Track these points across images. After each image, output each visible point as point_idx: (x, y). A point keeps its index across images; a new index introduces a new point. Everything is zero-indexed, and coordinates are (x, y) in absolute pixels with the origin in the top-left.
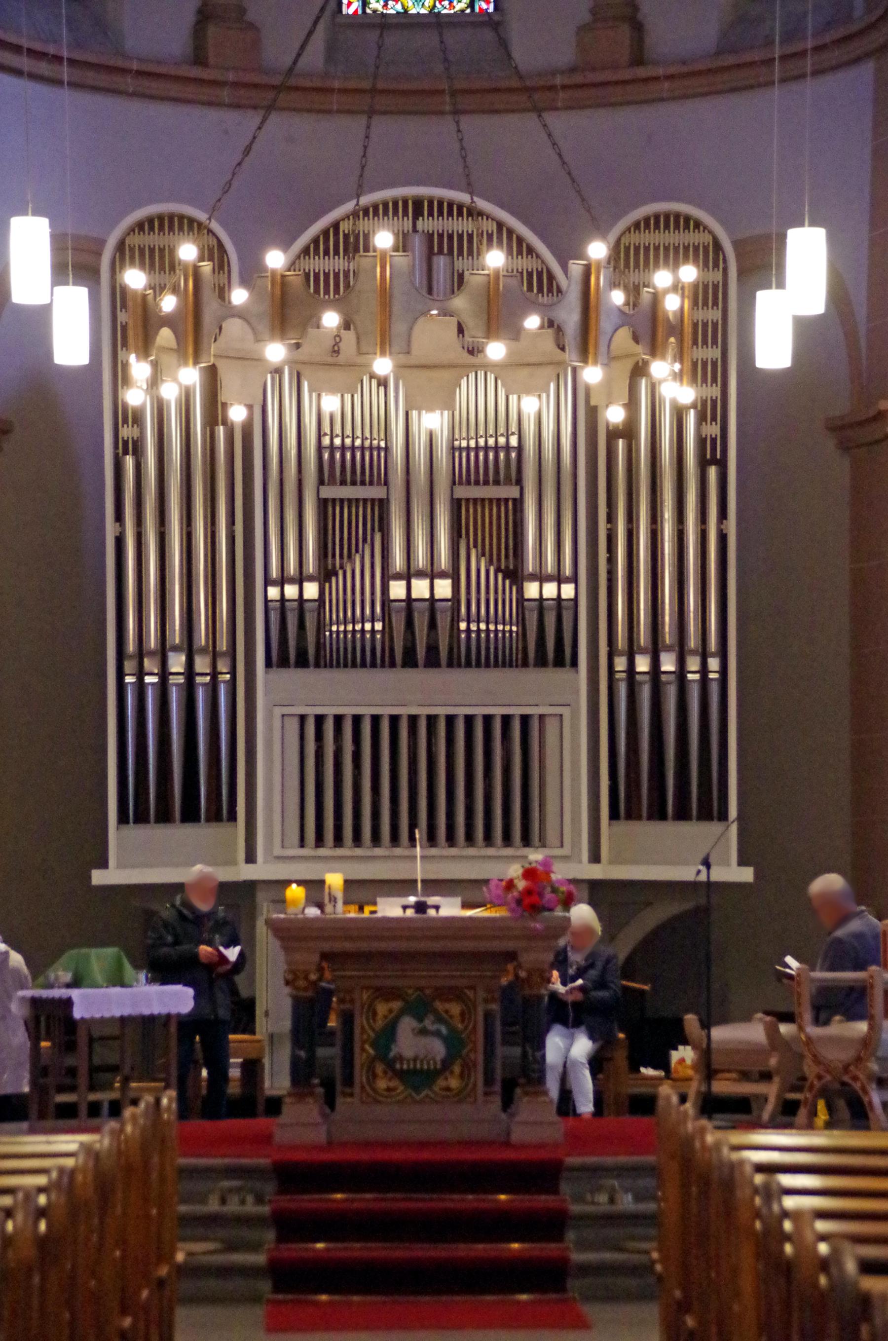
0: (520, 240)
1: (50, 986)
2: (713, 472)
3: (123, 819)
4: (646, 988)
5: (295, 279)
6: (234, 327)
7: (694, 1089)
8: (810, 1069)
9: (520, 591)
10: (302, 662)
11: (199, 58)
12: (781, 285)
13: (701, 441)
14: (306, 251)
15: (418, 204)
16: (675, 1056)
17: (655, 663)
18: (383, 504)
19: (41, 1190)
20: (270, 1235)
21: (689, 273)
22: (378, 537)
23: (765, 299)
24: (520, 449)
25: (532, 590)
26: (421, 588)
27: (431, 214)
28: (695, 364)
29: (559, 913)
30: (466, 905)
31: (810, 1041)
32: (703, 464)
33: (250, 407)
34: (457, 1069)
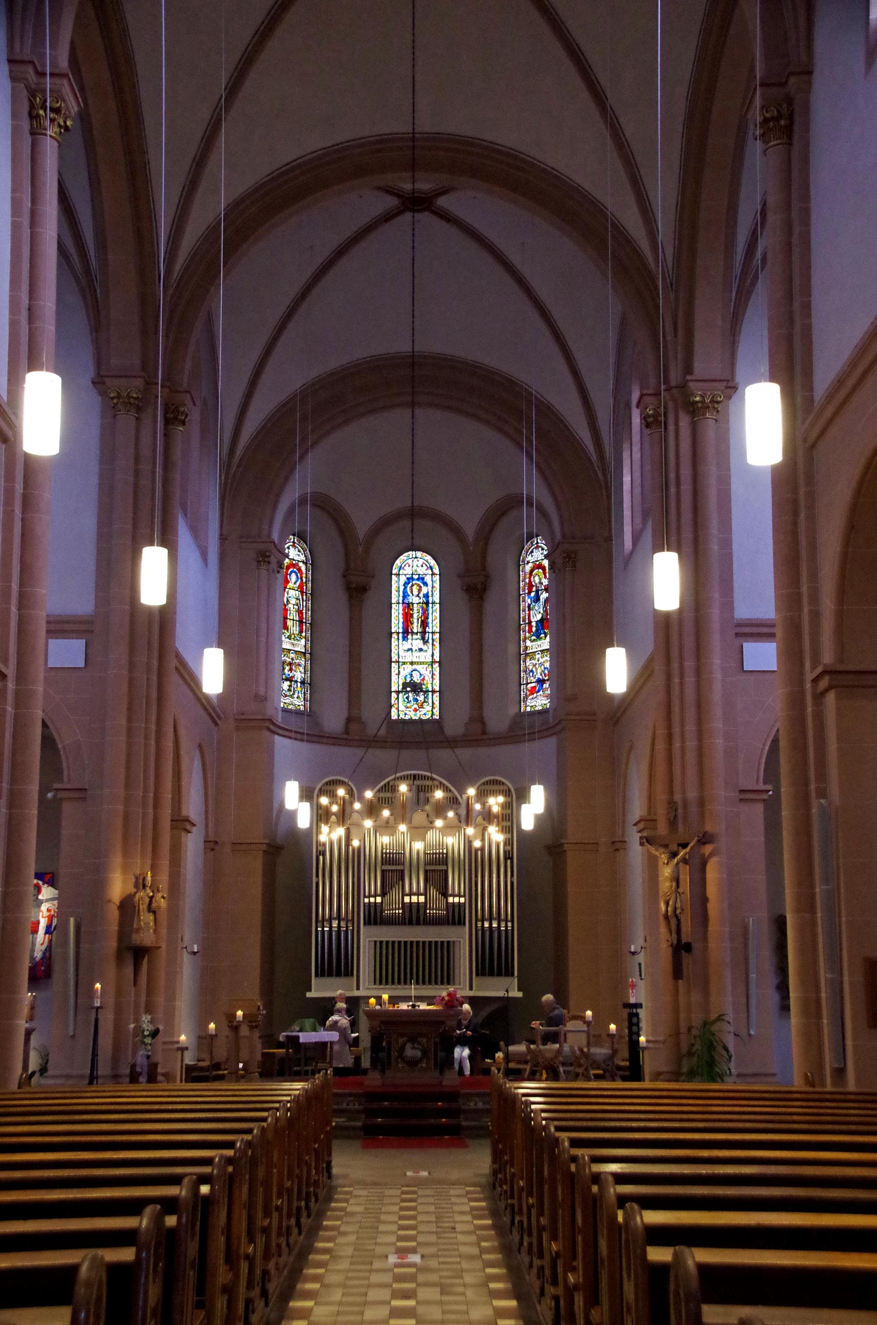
0: (447, 787)
1: (293, 1032)
2: (509, 862)
3: (317, 975)
4: (488, 1032)
5: (375, 800)
6: (355, 816)
7: (502, 1067)
8: (540, 1060)
9: (447, 900)
10: (375, 923)
11: (347, 732)
12: (529, 803)
13: (505, 852)
14: (379, 791)
15: (415, 776)
16: (497, 1055)
17: (491, 924)
18: (402, 872)
19: (288, 1102)
20: (364, 1116)
21: (501, 799)
22: (401, 883)
23: (524, 808)
24: (447, 854)
25: (451, 900)
26: (414, 899)
28: (503, 827)
29: (459, 1008)
30: (428, 1005)
31: (540, 1051)
32: (506, 859)
33: (360, 841)
34: (425, 1061)
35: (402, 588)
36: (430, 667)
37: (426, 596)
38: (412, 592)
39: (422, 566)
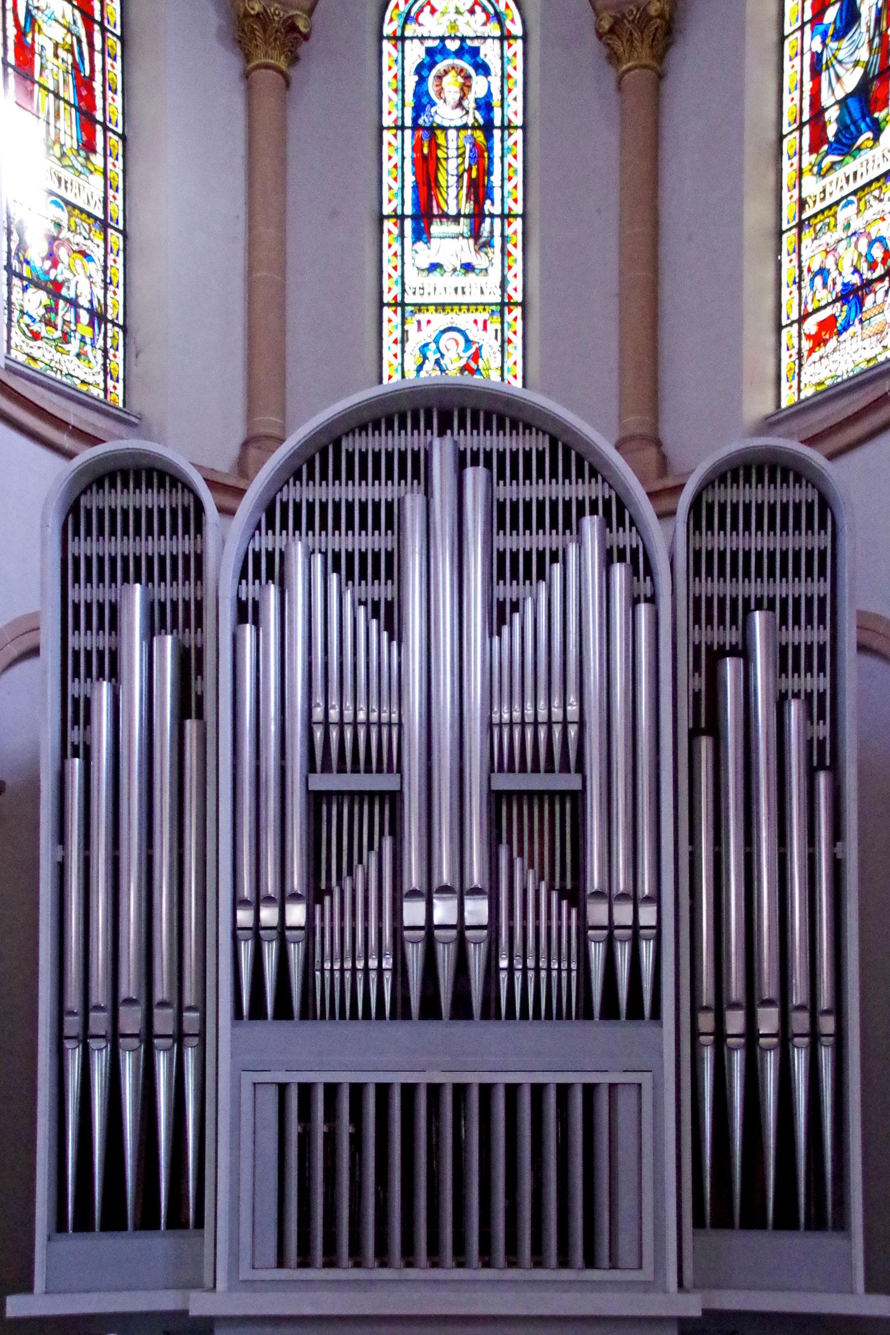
2: (822, 780)
9: (582, 916)
22: (388, 842)
27: (462, 426)
35: (411, 81)
36: (497, 318)
37: (485, 105)
38: (440, 93)
39: (472, 11)
